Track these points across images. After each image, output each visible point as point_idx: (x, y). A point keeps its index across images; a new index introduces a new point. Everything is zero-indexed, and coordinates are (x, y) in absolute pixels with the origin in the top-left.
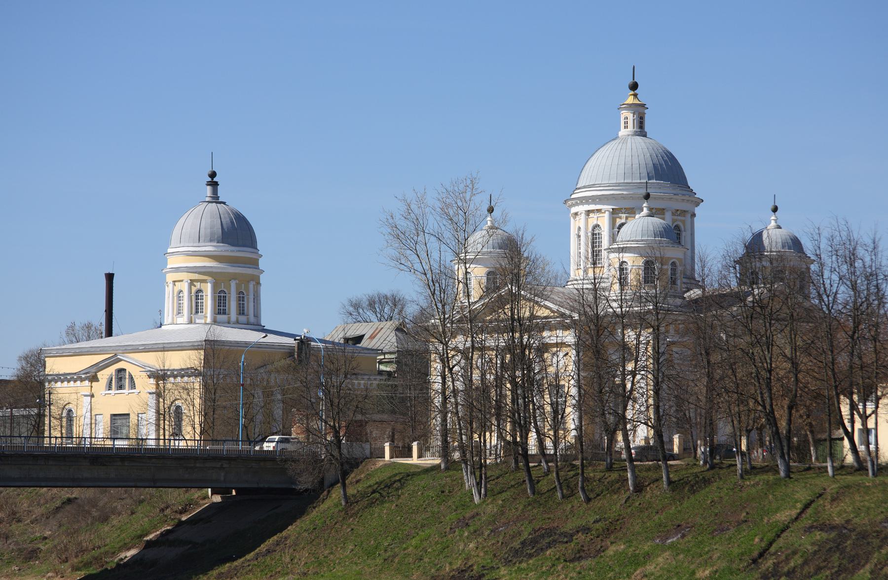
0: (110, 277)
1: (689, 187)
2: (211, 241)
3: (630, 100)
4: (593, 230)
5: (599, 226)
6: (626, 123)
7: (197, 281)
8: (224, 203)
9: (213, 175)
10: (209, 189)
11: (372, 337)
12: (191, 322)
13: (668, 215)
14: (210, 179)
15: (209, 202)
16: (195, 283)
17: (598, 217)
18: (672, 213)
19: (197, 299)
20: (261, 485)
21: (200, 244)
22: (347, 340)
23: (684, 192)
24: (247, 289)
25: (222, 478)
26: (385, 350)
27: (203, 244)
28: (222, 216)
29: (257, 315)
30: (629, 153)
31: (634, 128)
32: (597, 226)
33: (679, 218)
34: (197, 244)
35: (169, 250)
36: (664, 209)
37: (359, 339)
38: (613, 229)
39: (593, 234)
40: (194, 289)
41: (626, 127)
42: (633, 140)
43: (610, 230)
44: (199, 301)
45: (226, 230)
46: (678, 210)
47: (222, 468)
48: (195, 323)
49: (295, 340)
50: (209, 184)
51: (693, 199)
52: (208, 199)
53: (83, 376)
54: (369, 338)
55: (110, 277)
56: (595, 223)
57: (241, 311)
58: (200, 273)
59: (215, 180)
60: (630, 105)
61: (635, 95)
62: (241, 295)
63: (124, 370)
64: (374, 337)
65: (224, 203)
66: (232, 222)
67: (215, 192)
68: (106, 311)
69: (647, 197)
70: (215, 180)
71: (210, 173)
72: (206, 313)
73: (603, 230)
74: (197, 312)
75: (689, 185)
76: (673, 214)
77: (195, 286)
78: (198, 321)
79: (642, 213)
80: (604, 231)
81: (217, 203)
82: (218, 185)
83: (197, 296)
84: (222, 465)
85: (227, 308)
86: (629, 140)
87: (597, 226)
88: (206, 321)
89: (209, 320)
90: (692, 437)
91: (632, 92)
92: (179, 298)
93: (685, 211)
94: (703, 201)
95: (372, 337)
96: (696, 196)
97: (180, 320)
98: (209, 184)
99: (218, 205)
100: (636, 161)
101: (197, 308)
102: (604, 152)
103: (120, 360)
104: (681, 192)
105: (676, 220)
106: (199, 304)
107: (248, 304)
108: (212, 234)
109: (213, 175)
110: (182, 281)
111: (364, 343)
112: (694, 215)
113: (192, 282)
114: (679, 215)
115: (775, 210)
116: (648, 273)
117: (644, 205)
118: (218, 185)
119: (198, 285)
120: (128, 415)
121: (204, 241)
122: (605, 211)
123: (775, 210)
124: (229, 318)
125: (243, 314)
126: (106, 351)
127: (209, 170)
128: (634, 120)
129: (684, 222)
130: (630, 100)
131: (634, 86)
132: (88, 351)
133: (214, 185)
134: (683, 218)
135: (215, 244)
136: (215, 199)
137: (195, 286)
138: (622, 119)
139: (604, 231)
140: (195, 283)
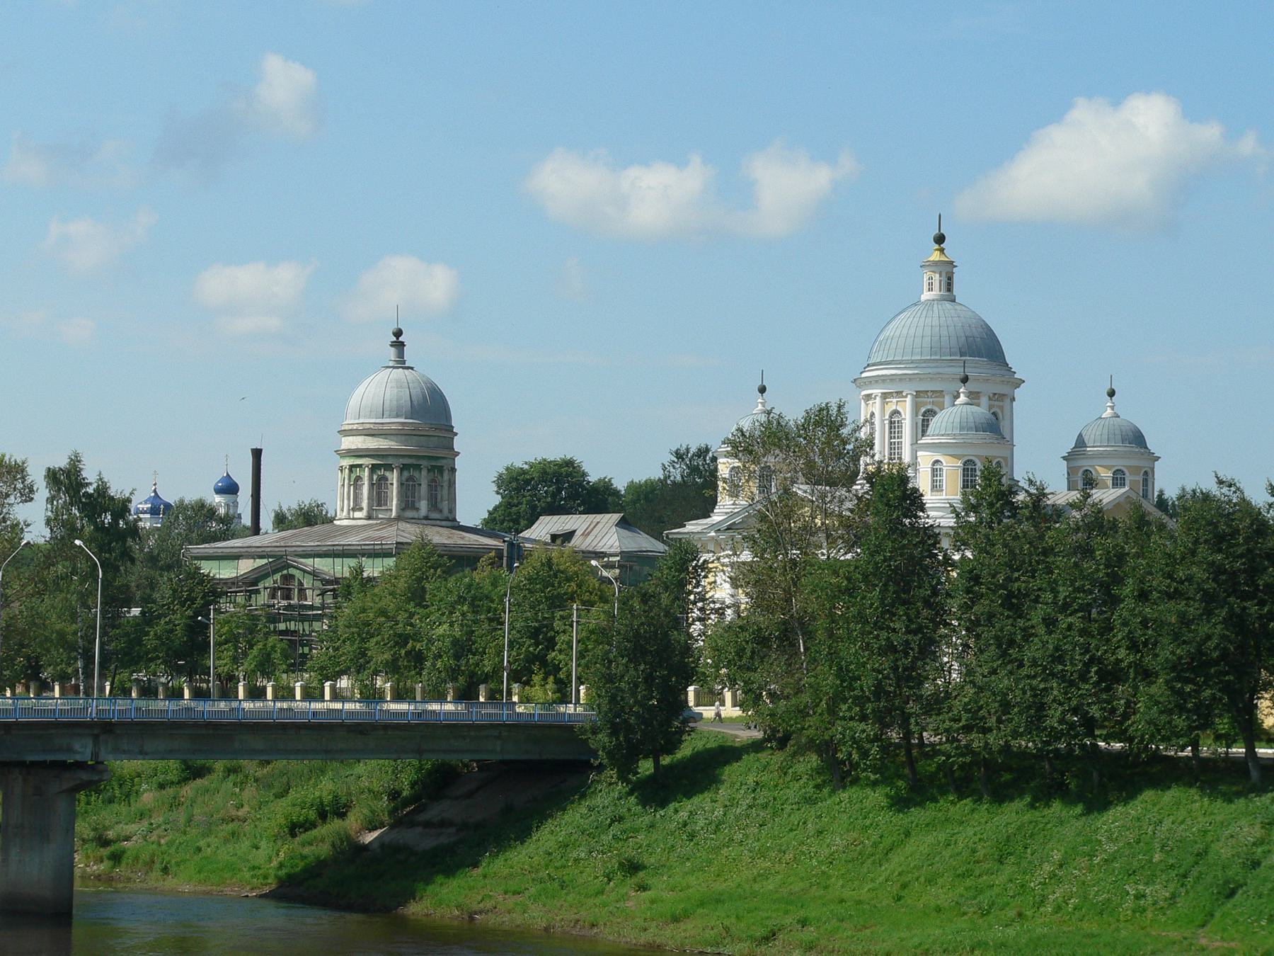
0: (257, 454)
1: (1008, 365)
3: (936, 256)
4: (891, 417)
5: (898, 412)
6: (931, 284)
8: (412, 368)
9: (398, 333)
10: (393, 350)
11: (586, 534)
13: (984, 400)
14: (395, 339)
15: (394, 367)
17: (897, 402)
18: (989, 397)
20: (544, 757)
22: (554, 537)
23: (1002, 372)
25: (499, 749)
26: (609, 551)
28: (410, 385)
29: (452, 510)
30: (936, 322)
31: (940, 291)
32: (896, 412)
33: (996, 403)
36: (978, 393)
37: (569, 536)
38: (917, 416)
39: (891, 422)
41: (930, 289)
42: (940, 306)
43: (912, 418)
46: (995, 394)
47: (499, 737)
49: (504, 541)
50: (393, 344)
51: (1012, 380)
52: (391, 364)
54: (582, 534)
55: (257, 454)
56: (894, 408)
57: (434, 505)
59: (401, 339)
60: (936, 263)
61: (942, 251)
64: (589, 534)
65: (412, 368)
66: (423, 393)
67: (401, 354)
68: (252, 496)
69: (965, 380)
70: (401, 339)
73: (903, 417)
75: (1008, 362)
76: (990, 399)
79: (959, 400)
80: (905, 419)
81: (403, 368)
82: (404, 345)
84: (500, 733)
86: (935, 306)
87: (896, 412)
91: (937, 246)
93: (1004, 395)
94: (1024, 382)
95: (586, 534)
96: (1016, 376)
97: (357, 514)
98: (393, 344)
99: (406, 371)
100: (944, 333)
101: (379, 498)
102: (905, 320)
104: (998, 372)
105: (994, 406)
109: (398, 333)
111: (576, 542)
112: (1013, 399)
114: (997, 400)
115: (1112, 394)
116: (898, 448)
117: (961, 390)
118: (404, 345)
122: (907, 394)
123: (1112, 394)
127: (394, 327)
128: (940, 281)
129: (1001, 408)
130: (936, 256)
131: (940, 239)
133: (399, 345)
134: (1001, 404)
136: (401, 363)
138: (925, 279)
139: (905, 419)
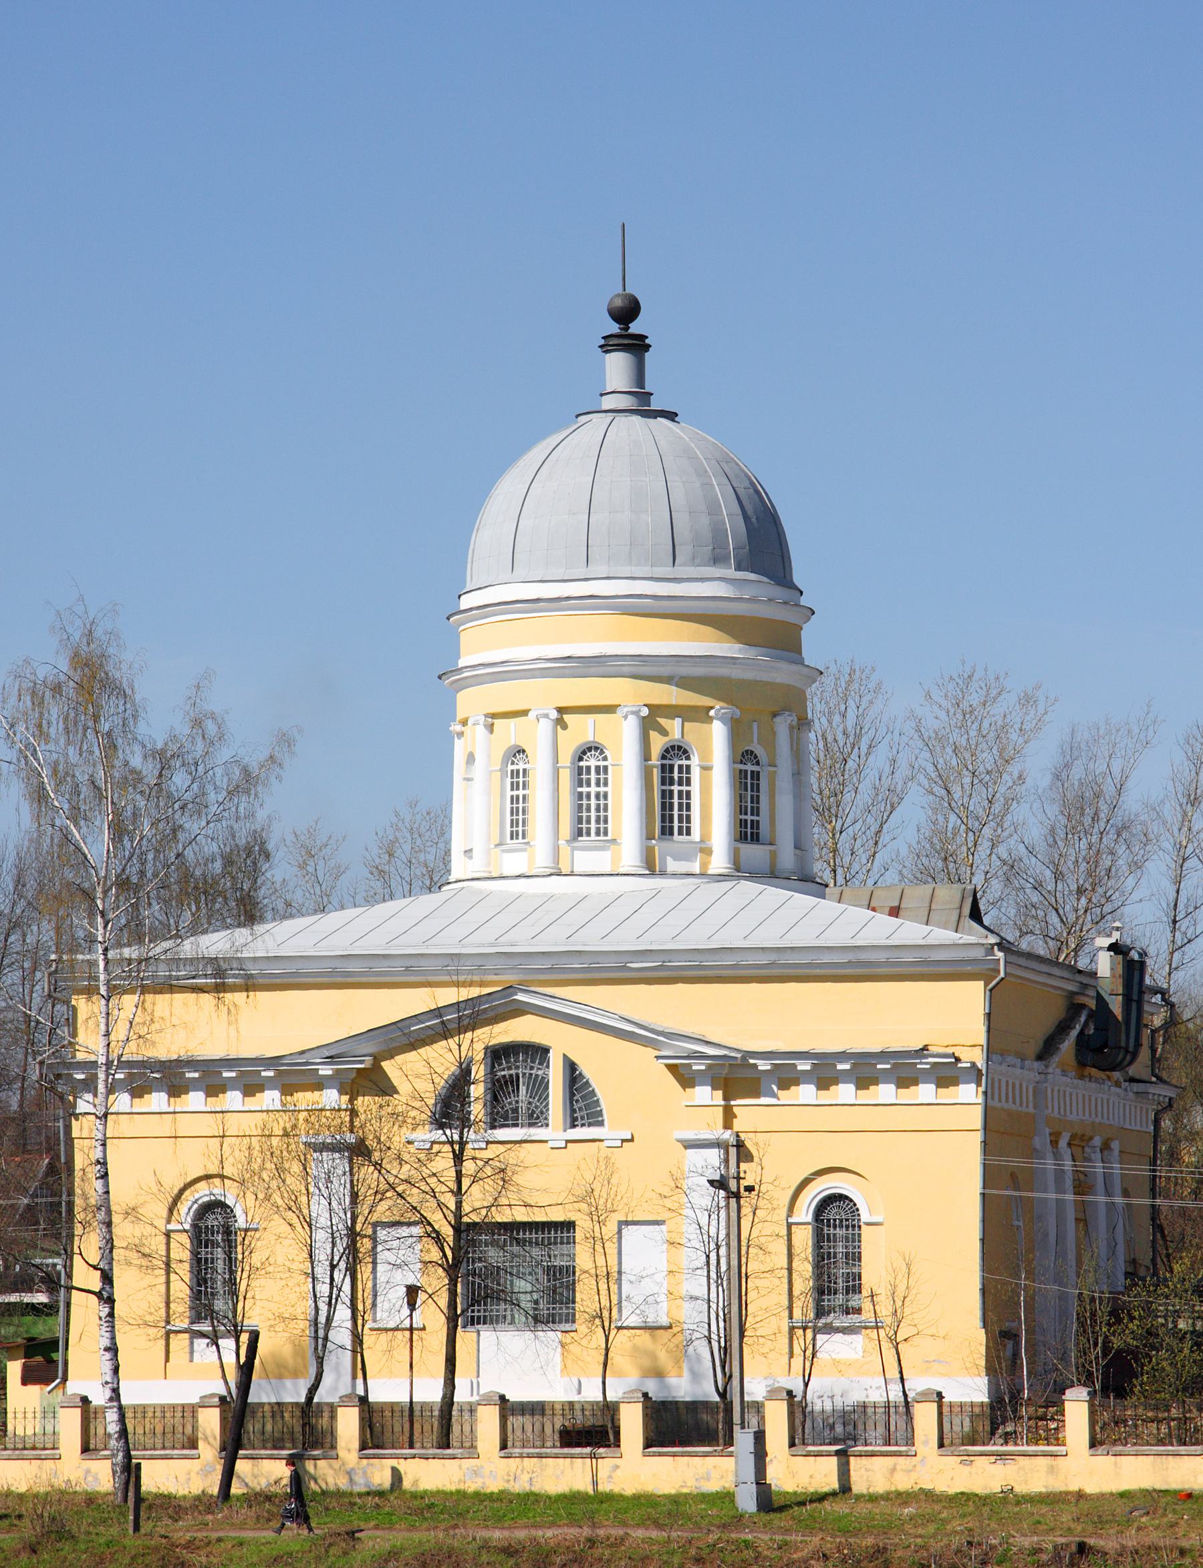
2: (717, 559)
7: (672, 711)
9: (627, 312)
12: (651, 866)
14: (615, 328)
16: (662, 721)
19: (667, 780)
21: (681, 571)
24: (770, 742)
27: (692, 571)
34: (667, 571)
35: (466, 602)
40: (658, 743)
44: (676, 788)
45: (754, 520)
48: (663, 874)
53: (326, 1071)
58: (685, 683)
59: (635, 328)
62: (749, 767)
63: (539, 1053)
70: (635, 328)
71: (619, 303)
72: (706, 837)
74: (667, 831)
77: (664, 732)
78: (672, 866)
83: (666, 770)
85: (764, 818)
88: (704, 865)
89: (719, 862)
90: (244, 1239)
92: (519, 780)
103: (520, 1010)
106: (676, 801)
107: (772, 796)
108: (718, 533)
109: (627, 312)
110: (610, 709)
113: (651, 721)
119: (674, 727)
120: (569, 1226)
121: (693, 561)
124: (773, 856)
125: (755, 838)
126: (349, 974)
127: (609, 292)
132: (333, 973)
135: (731, 573)
137: (664, 732)
140: (662, 721)
